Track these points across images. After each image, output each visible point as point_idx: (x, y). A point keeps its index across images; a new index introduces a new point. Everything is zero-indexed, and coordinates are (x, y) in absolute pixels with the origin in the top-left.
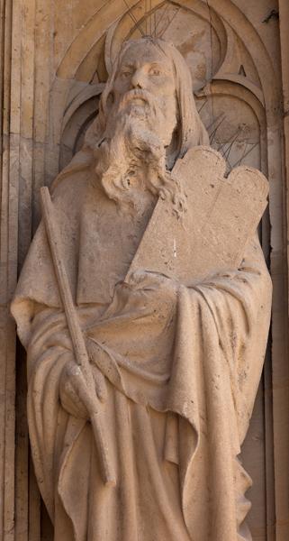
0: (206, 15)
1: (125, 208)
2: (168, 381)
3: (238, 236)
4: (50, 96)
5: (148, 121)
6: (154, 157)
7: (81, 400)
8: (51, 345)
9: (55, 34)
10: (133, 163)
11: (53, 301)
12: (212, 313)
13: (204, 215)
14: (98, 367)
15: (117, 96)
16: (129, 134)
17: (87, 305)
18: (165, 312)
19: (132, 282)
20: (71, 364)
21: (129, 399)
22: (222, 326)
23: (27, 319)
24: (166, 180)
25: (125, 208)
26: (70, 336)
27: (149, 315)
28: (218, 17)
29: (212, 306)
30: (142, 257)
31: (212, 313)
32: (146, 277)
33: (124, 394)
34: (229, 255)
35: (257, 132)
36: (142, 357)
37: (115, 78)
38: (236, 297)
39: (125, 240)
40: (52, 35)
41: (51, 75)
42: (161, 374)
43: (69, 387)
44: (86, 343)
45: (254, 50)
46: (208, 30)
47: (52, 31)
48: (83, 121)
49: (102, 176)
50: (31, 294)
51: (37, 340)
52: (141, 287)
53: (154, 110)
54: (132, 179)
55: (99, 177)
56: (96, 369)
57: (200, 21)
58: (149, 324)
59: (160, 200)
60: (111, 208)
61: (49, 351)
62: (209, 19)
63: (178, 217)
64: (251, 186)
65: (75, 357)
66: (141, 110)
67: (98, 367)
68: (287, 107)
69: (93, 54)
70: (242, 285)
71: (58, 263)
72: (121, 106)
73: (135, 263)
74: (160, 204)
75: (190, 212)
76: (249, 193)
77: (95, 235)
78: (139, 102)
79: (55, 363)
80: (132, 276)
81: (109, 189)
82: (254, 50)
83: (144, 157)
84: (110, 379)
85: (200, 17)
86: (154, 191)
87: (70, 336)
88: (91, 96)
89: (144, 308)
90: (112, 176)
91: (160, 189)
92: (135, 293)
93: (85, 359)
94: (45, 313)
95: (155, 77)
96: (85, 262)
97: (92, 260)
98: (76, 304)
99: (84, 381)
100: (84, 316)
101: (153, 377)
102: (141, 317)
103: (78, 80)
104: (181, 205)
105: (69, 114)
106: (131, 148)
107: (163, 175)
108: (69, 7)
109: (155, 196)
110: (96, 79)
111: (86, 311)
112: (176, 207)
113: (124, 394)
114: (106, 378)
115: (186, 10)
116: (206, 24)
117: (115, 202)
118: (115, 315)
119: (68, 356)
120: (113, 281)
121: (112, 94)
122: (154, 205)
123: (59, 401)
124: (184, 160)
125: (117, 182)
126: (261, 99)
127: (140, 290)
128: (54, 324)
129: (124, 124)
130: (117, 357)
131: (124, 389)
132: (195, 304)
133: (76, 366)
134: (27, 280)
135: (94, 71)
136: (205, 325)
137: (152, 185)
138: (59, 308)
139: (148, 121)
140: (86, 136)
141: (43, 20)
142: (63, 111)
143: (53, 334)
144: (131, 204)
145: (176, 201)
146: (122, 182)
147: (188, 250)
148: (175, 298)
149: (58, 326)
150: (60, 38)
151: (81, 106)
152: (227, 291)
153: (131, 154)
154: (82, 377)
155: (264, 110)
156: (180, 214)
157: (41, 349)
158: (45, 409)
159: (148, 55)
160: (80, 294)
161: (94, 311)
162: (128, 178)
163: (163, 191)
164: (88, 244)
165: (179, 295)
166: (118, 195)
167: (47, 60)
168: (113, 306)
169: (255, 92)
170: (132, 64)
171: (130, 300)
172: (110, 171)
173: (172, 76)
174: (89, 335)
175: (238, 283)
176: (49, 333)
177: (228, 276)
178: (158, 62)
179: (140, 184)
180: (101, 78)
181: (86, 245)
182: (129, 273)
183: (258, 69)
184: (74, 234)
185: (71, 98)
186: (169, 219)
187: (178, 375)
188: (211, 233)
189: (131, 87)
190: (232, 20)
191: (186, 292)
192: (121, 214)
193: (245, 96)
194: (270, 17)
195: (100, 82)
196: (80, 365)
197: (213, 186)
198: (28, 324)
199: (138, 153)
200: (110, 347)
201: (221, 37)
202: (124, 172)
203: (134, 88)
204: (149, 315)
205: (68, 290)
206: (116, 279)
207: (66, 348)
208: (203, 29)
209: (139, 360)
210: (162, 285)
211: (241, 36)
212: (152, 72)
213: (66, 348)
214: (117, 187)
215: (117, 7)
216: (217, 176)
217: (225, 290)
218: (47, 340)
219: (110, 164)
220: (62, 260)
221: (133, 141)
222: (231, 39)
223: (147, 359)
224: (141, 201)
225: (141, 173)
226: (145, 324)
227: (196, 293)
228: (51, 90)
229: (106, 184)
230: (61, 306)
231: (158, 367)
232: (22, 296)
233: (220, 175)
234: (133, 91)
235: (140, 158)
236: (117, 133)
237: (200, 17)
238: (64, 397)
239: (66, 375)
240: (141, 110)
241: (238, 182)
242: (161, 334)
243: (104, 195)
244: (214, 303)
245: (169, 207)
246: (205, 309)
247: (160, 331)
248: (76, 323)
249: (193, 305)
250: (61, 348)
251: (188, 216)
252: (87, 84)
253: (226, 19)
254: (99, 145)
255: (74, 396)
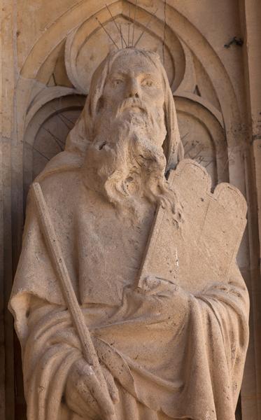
0: (160, 33)
1: (125, 213)
2: (182, 388)
3: (226, 251)
4: (15, 93)
5: (147, 130)
6: (159, 165)
7: (96, 400)
8: (56, 342)
9: (18, 34)
10: (134, 169)
11: (55, 297)
12: (220, 325)
13: (198, 227)
14: (109, 369)
15: (109, 104)
16: (134, 140)
17: (92, 305)
18: (178, 319)
19: (146, 288)
20: (82, 363)
21: (140, 403)
22: (227, 338)
23: (25, 313)
24: (165, 189)
25: (125, 213)
26: (77, 333)
27: (163, 321)
28: (174, 36)
29: (219, 318)
30: (150, 263)
31: (220, 325)
32: (160, 284)
33: (135, 397)
34: (220, 268)
35: (210, 151)
36: (152, 361)
37: (105, 84)
38: (236, 312)
39: (127, 244)
40: (15, 35)
41: (15, 73)
42: (172, 380)
43: (82, 386)
44: (95, 343)
45: (212, 71)
46: (161, 48)
47: (16, 30)
48: (42, 121)
49: (107, 179)
50: (34, 289)
51: (40, 336)
52: (154, 292)
53: (152, 120)
54: (130, 184)
55: (101, 181)
56: (105, 369)
57: (153, 39)
58: (161, 330)
59: (161, 209)
60: (109, 212)
61: (55, 348)
62: (163, 39)
63: (178, 227)
64: (233, 203)
65: (84, 355)
66: (140, 119)
67: (109, 369)
68: (256, 130)
69: (52, 58)
70: (237, 298)
71: (58, 260)
72: (118, 112)
73: (145, 267)
74: (161, 213)
75: (187, 223)
76: (232, 210)
77: (95, 236)
78: (137, 110)
79: (63, 360)
80: (145, 281)
81: (111, 193)
82: (212, 71)
83: (146, 164)
84: (121, 381)
85: (153, 34)
86: (153, 199)
87: (77, 333)
88: (53, 98)
89: (158, 314)
90: (115, 180)
91: (159, 198)
92: (149, 297)
93: (96, 359)
94: (44, 310)
95: (147, 87)
96: (88, 263)
97: (96, 262)
98: (80, 303)
99: (98, 381)
100: (90, 316)
101: (167, 383)
102: (155, 323)
103: (38, 81)
104: (180, 215)
105: (32, 113)
106: (133, 154)
107: (163, 184)
108: (32, 8)
109: (154, 206)
110: (52, 82)
111: (91, 311)
112: (175, 216)
113: (135, 397)
114: (116, 380)
115: (138, 25)
116: (159, 42)
117: (114, 206)
118: (125, 318)
119: (76, 356)
120: (121, 284)
121: (102, 100)
122: (155, 213)
123: (64, 400)
124: (177, 172)
125: (119, 186)
126: (221, 120)
127: (154, 295)
128: (59, 322)
129: (128, 130)
130: (128, 359)
131: (136, 392)
132: (205, 315)
133: (87, 366)
134: (28, 275)
135: (51, 74)
136: (215, 336)
137: (151, 193)
138: (59, 306)
139: (147, 130)
140: (71, 138)
141: (6, 18)
142: (26, 109)
143: (58, 332)
144: (132, 210)
145: (176, 211)
146: (122, 186)
147: (188, 261)
148: (187, 307)
149: (63, 323)
150: (22, 38)
151: (43, 106)
152: (227, 304)
153: (134, 161)
154: (95, 377)
155: (223, 132)
156: (180, 224)
157: (45, 344)
158: (50, 405)
159: (140, 65)
160: (86, 294)
161: (101, 312)
162: (127, 184)
163: (164, 201)
164: (90, 244)
165: (191, 305)
166: (118, 199)
167: (11, 57)
168: (124, 309)
169: (213, 113)
170: (126, 72)
171: (144, 305)
172: (115, 176)
173: (162, 89)
174: (96, 336)
175: (234, 297)
176: (53, 330)
177: (224, 289)
178: (152, 73)
179: (137, 191)
180: (57, 82)
181: (87, 247)
182: (142, 278)
183: (217, 91)
184: (68, 233)
185: (32, 97)
186: (170, 228)
187: (198, 384)
188: (204, 245)
189: (128, 95)
190: (190, 41)
191: (197, 302)
192: (121, 219)
193: (201, 115)
194: (231, 43)
195: (56, 85)
196: (91, 364)
197: (203, 200)
198: (25, 318)
199: (141, 160)
200: (120, 349)
201: (175, 55)
202: (125, 177)
203: (131, 96)
204: (163, 321)
205: (72, 288)
206: (123, 283)
207: (73, 346)
208: (155, 46)
209: (149, 365)
210: (175, 294)
211: (199, 56)
212: (145, 83)
213: (73, 346)
214: (117, 191)
215: (77, 15)
216: (205, 190)
217: (227, 303)
218: (52, 337)
219: (116, 168)
220: (62, 258)
221: (139, 148)
222: (189, 59)
223: (158, 363)
224: (142, 209)
225: (139, 180)
226: (156, 330)
227: (205, 305)
228: (15, 88)
229: (108, 187)
230: (63, 303)
231: (170, 373)
232: (25, 290)
233: (207, 189)
234: (131, 100)
235: (141, 165)
236: (121, 138)
237: (153, 34)
238: (73, 395)
239: (76, 374)
240: (140, 119)
241: (223, 199)
242: (171, 341)
243: (104, 198)
244: (221, 315)
245: (169, 216)
246: (214, 320)
247: (170, 338)
248: (84, 322)
249: (203, 316)
250: (68, 346)
251: (185, 226)
252: (44, 85)
253: (185, 39)
254: (101, 148)
255: (87, 395)
